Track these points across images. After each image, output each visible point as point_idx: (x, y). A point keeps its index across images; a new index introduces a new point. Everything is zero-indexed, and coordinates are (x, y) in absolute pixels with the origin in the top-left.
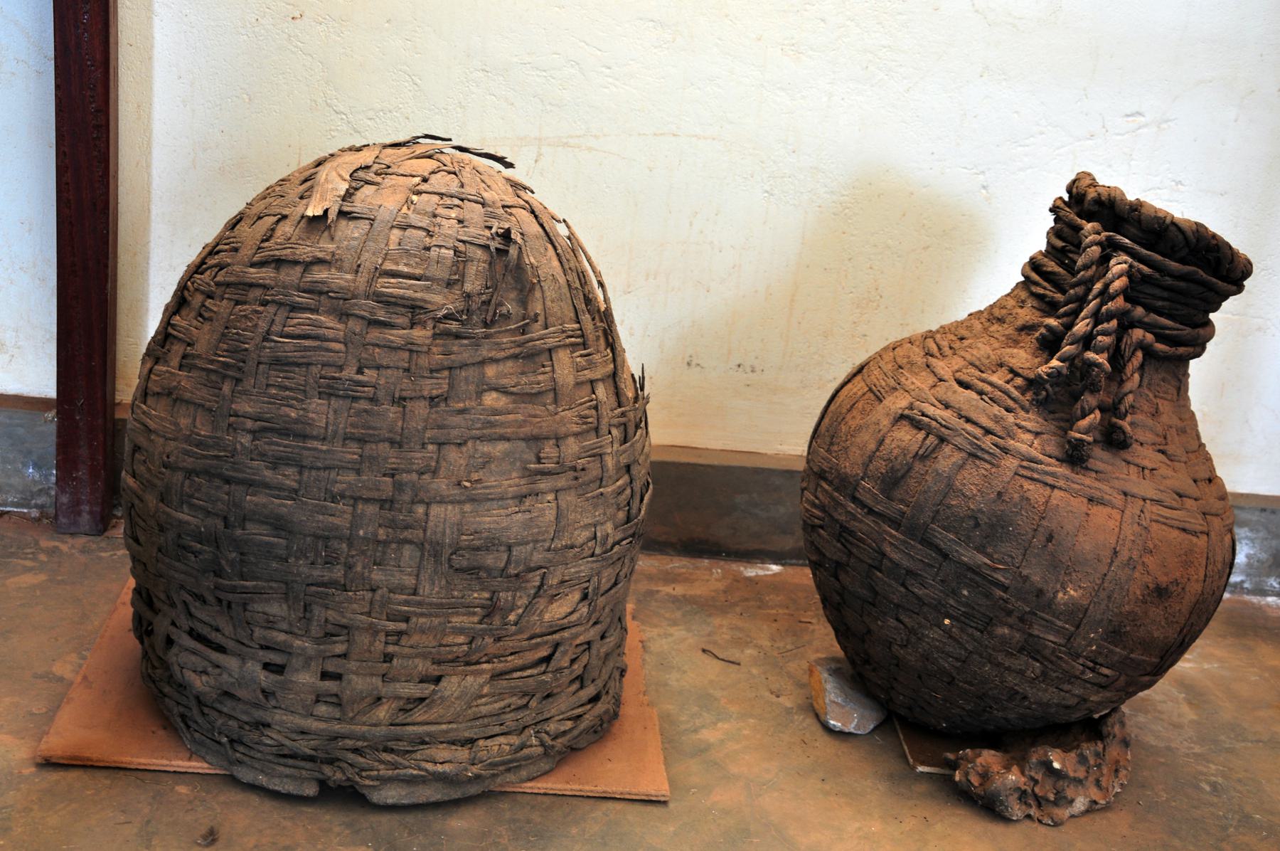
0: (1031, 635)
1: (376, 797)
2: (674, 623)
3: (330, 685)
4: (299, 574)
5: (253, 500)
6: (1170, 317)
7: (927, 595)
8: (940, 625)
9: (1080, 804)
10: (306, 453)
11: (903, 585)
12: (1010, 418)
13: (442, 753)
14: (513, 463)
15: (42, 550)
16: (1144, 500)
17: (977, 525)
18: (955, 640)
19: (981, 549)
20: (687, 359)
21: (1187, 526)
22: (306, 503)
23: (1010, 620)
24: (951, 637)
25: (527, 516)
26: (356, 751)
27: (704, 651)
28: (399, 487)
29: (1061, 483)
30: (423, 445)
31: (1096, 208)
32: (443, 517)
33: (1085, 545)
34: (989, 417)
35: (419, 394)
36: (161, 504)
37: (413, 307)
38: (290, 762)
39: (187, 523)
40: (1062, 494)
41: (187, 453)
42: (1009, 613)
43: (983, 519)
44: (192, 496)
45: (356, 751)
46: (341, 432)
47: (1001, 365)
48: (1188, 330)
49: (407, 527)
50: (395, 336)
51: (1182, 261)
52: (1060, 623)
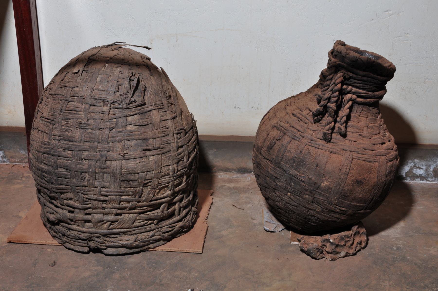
1: (105, 252)
2: (226, 196)
3: (88, 217)
4: (74, 183)
5: (60, 161)
6: (363, 89)
8: (287, 195)
9: (343, 254)
10: (73, 146)
11: (275, 182)
12: (306, 126)
13: (125, 237)
14: (138, 147)
15: (24, 177)
17: (294, 162)
19: (296, 169)
20: (234, 106)
21: (368, 160)
22: (74, 162)
23: (307, 193)
24: (290, 199)
25: (144, 163)
26: (98, 237)
28: (101, 156)
29: (321, 147)
30: (108, 143)
31: (337, 54)
32: (115, 164)
33: (329, 167)
34: (299, 126)
35: (106, 127)
36: (37, 163)
37: (104, 100)
38: (79, 241)
39: (43, 168)
41: (42, 147)
42: (306, 190)
43: (296, 160)
44: (44, 160)
45: (98, 237)
46: (83, 139)
47: (307, 108)
48: (370, 93)
49: (105, 168)
50: (98, 109)
51: (364, 71)
52: (324, 193)
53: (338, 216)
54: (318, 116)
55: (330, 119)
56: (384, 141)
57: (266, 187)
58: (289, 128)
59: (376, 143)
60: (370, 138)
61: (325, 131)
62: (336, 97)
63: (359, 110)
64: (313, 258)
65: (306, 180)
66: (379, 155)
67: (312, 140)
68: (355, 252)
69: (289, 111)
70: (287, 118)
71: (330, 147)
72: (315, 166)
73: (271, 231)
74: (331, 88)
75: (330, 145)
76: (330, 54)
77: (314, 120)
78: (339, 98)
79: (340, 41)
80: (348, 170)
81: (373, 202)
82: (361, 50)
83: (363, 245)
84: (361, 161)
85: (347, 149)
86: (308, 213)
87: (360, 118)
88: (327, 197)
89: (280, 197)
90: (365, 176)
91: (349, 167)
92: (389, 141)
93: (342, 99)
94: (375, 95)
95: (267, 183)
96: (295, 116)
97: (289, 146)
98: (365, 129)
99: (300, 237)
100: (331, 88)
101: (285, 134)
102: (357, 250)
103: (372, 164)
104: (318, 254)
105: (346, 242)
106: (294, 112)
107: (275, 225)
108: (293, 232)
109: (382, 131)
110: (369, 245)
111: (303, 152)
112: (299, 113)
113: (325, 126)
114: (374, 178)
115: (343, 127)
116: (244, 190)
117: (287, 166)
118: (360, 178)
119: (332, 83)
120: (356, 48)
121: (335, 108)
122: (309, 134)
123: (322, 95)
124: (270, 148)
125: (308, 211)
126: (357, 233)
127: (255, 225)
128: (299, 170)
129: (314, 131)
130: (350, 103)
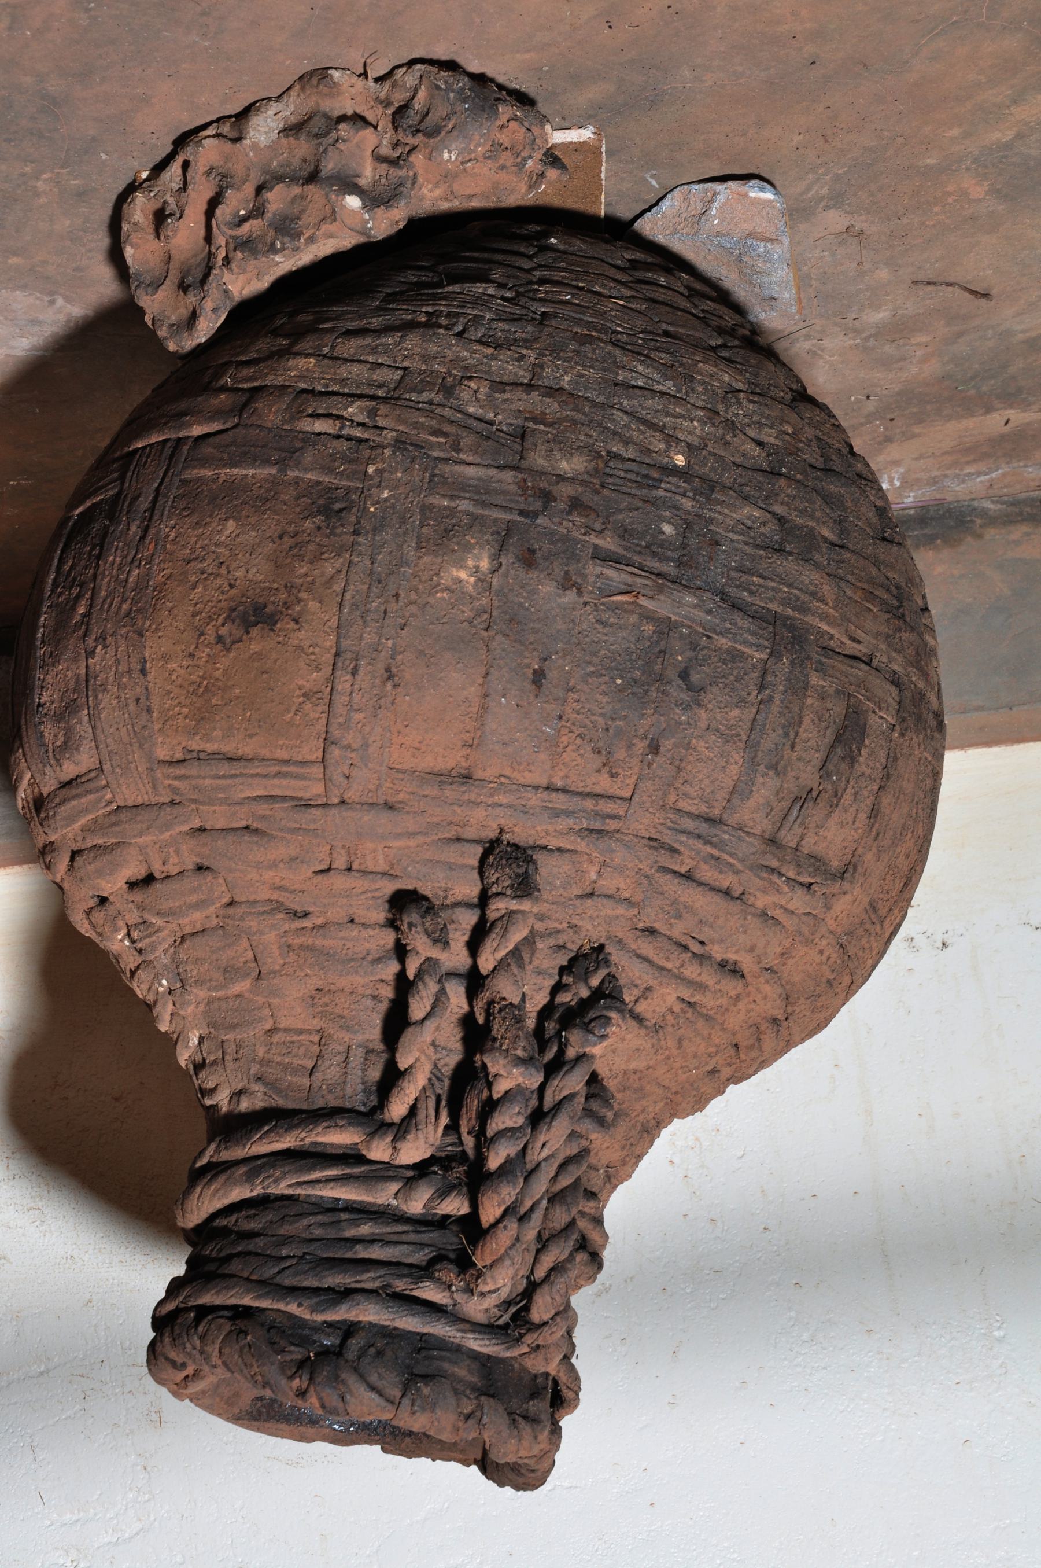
0: (516, 468)
6: (334, 1207)
7: (733, 507)
8: (690, 450)
9: (264, 129)
11: (781, 520)
12: (651, 917)
16: (343, 802)
17: (684, 675)
18: (653, 426)
19: (666, 627)
21: (225, 768)
23: (567, 490)
27: (986, 296)
29: (534, 799)
33: (461, 682)
40: (529, 778)
42: (575, 505)
43: (676, 691)
47: (657, 1028)
48: (282, 1188)
51: (349, 1329)
52: (464, 505)
53: (345, 371)
54: (589, 992)
55: (506, 989)
56: (138, 896)
57: (827, 470)
58: (752, 882)
59: (192, 881)
60: (231, 904)
61: (526, 905)
62: (501, 1134)
63: (330, 1071)
64: (451, 66)
65: (594, 569)
66: (160, 805)
67: (600, 832)
68: (187, 153)
69: (767, 989)
70: (772, 945)
71: (480, 813)
72: (552, 674)
73: (732, 185)
74: (540, 1186)
75: (484, 822)
76: (568, 1394)
77: (607, 962)
78: (480, 1134)
79: (518, 1488)
80: (344, 683)
81: (144, 503)
82: (371, 1442)
83: (140, 210)
84: (265, 753)
85: (368, 818)
86: (531, 355)
87: (316, 1023)
88: (434, 483)
89: (730, 425)
90: (224, 662)
91: (340, 700)
92: (103, 900)
93: (453, 1127)
94: (250, 1177)
95: (827, 499)
96: (723, 964)
97: (734, 770)
98: (273, 959)
99: (550, 190)
100: (540, 1186)
101: (772, 841)
102: (175, 168)
103: (195, 744)
104: (422, 94)
105: (257, 211)
106: (731, 986)
107: (701, 223)
108: (591, 209)
109: (161, 956)
110: (105, 213)
111: (640, 746)
112: (700, 987)
113: (529, 941)
114: (166, 658)
115: (422, 947)
116: (915, 407)
117: (724, 642)
118: (254, 647)
119: (537, 1217)
120: (409, 1454)
121: (495, 1064)
122: (621, 869)
123: (586, 1126)
124: (849, 734)
125: (536, 369)
126: (196, 278)
127: (836, 200)
128: (649, 628)
129: (591, 895)
130: (397, 1109)
